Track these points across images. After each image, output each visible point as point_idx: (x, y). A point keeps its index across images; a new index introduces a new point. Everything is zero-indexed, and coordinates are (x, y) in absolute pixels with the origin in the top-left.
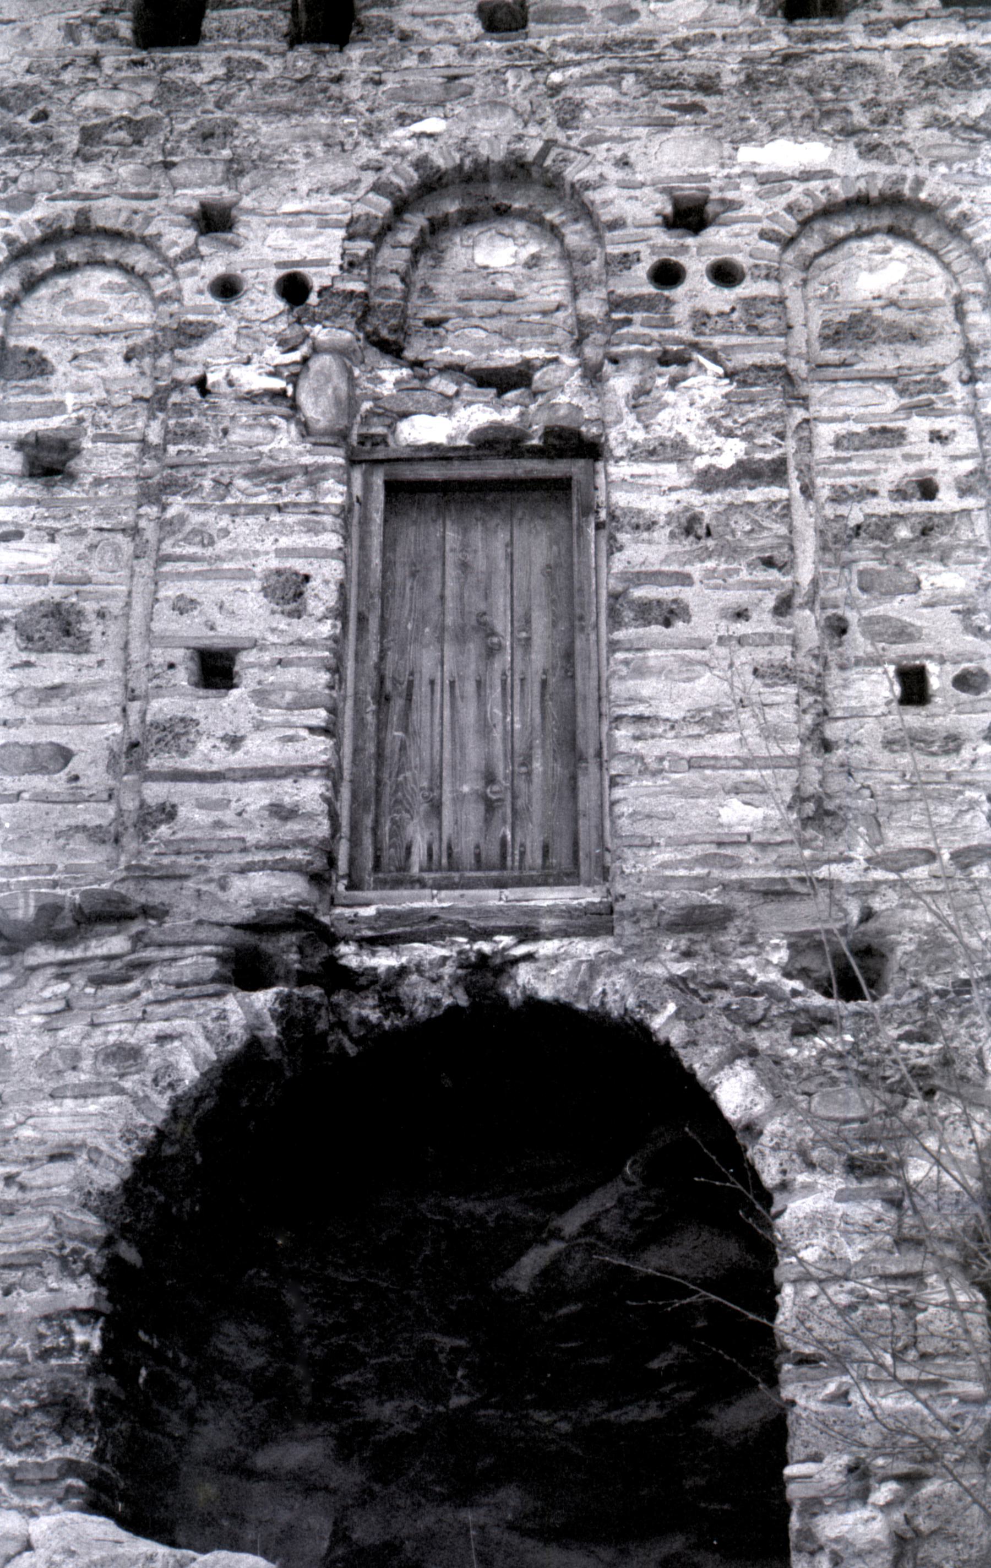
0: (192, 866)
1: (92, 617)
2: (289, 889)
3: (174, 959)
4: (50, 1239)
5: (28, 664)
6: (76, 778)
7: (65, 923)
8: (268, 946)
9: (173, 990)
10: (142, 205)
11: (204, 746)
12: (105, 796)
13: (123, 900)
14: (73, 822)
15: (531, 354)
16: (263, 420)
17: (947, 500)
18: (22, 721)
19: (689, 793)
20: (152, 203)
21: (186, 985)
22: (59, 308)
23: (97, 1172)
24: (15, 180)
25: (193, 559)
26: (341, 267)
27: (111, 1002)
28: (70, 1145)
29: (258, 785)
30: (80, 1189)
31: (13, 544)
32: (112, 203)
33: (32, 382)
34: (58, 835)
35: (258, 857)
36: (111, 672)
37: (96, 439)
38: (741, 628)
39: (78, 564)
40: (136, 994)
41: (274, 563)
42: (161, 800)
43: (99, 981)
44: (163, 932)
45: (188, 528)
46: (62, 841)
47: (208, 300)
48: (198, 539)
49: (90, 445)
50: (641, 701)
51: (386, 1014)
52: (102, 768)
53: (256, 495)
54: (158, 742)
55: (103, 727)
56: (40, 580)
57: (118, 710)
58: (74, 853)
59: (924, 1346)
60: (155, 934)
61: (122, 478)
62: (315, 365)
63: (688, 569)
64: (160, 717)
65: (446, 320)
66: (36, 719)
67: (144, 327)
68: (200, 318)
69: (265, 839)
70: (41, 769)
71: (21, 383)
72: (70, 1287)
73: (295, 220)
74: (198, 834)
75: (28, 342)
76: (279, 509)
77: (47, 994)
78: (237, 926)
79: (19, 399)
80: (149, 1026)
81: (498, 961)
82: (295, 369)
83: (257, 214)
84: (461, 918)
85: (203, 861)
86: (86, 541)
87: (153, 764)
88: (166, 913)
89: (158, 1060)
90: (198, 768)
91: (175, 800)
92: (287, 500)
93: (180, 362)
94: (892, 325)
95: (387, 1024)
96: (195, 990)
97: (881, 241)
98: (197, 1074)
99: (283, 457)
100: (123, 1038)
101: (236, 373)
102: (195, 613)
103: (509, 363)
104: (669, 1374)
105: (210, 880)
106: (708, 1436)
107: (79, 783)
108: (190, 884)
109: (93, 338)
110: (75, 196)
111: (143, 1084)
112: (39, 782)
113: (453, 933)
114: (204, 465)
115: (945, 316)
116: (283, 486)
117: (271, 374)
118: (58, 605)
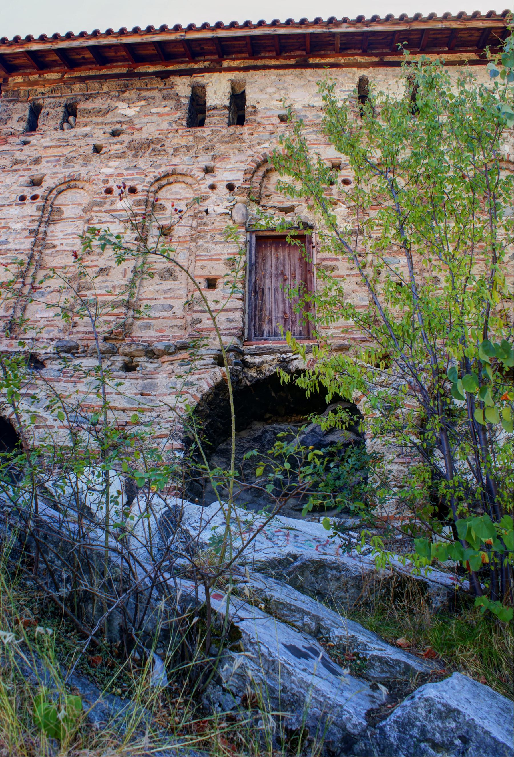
7: (172, 350)
10: (190, 167)
32: (182, 167)
38: (352, 272)
47: (208, 190)
70: (165, 311)
72: (175, 443)
73: (231, 170)
87: (195, 308)
101: (216, 208)
112: (165, 314)
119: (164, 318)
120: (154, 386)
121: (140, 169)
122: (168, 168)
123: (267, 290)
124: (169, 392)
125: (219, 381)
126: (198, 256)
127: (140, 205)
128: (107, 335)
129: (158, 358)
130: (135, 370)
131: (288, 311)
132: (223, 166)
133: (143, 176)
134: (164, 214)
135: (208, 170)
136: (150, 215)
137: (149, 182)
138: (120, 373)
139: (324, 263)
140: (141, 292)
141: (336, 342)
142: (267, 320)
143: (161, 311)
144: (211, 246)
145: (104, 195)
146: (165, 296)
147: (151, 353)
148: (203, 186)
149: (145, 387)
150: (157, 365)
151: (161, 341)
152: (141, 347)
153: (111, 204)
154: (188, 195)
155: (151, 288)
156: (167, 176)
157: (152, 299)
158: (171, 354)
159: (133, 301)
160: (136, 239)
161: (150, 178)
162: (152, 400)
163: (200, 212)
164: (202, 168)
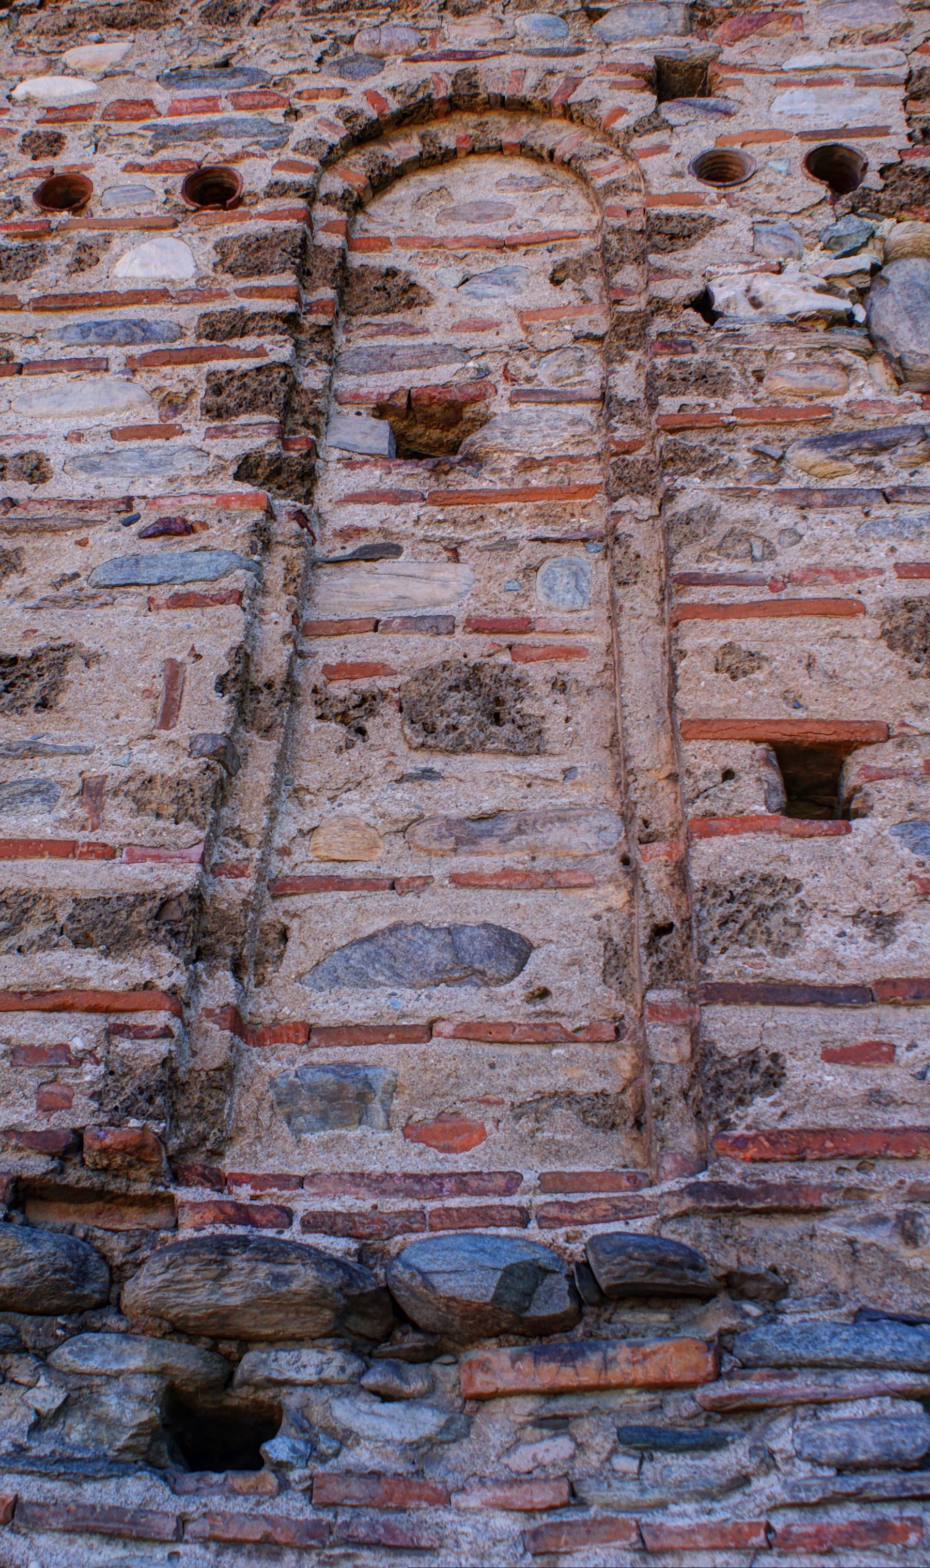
0: (831, 1188)
3: (821, 1403)
5: (428, 774)
6: (544, 994)
7: (554, 1301)
10: (564, 64)
11: (821, 932)
12: (608, 1031)
13: (694, 1261)
14: (546, 1084)
16: (825, 356)
18: (427, 881)
20: (579, 60)
21: (860, 1468)
22: (430, 214)
24: (351, 41)
25: (739, 581)
26: (910, 137)
27: (680, 1498)
31: (383, 566)
32: (510, 62)
33: (395, 318)
34: (519, 1111)
36: (593, 788)
37: (516, 398)
39: (508, 598)
40: (742, 1481)
41: (899, 589)
42: (749, 1044)
43: (645, 1442)
44: (784, 1337)
45: (721, 529)
46: (526, 1125)
47: (692, 185)
48: (742, 548)
49: (506, 408)
52: (593, 976)
53: (833, 475)
54: (724, 923)
55: (589, 893)
56: (440, 626)
57: (612, 863)
58: (556, 1151)
61: (571, 459)
62: (895, 273)
64: (719, 875)
67: (574, 236)
68: (684, 210)
71: (376, 319)
73: (815, 79)
74: (836, 1121)
75: (380, 260)
76: (887, 497)
77: (521, 1460)
79: (375, 342)
82: (863, 282)
83: (752, 70)
85: (854, 1178)
86: (518, 560)
87: (720, 968)
88: (783, 1291)
90: (818, 978)
91: (774, 1044)
92: (895, 482)
93: (660, 273)
96: (889, 1481)
99: (873, 414)
101: (764, 285)
102: (759, 676)
105: (880, 1220)
107: (553, 1004)
108: (830, 1226)
109: (493, 253)
110: (450, 55)
112: (468, 1002)
114: (729, 427)
116: (883, 459)
117: (820, 290)
118: (477, 668)
121: (254, 75)
122: (426, 69)
126: (691, 580)
127: (260, 270)
128: (37, 1165)
129: (425, 1356)
130: (253, 1461)
132: (763, 59)
133: (276, 116)
134: (409, 330)
135: (673, 82)
136: (325, 332)
137: (310, 145)
138: (136, 1490)
140: (288, 828)
143: (442, 977)
144: (769, 516)
145: (31, 213)
146: (463, 863)
147: (380, 1322)
148: (654, 165)
151: (462, 1219)
152: (304, 1278)
153: (79, 265)
154: (558, 223)
155: (354, 805)
156: (417, 112)
157: (370, 884)
159: (232, 891)
160: (246, 470)
161: (319, 124)
163: (659, 306)
164: (638, 71)
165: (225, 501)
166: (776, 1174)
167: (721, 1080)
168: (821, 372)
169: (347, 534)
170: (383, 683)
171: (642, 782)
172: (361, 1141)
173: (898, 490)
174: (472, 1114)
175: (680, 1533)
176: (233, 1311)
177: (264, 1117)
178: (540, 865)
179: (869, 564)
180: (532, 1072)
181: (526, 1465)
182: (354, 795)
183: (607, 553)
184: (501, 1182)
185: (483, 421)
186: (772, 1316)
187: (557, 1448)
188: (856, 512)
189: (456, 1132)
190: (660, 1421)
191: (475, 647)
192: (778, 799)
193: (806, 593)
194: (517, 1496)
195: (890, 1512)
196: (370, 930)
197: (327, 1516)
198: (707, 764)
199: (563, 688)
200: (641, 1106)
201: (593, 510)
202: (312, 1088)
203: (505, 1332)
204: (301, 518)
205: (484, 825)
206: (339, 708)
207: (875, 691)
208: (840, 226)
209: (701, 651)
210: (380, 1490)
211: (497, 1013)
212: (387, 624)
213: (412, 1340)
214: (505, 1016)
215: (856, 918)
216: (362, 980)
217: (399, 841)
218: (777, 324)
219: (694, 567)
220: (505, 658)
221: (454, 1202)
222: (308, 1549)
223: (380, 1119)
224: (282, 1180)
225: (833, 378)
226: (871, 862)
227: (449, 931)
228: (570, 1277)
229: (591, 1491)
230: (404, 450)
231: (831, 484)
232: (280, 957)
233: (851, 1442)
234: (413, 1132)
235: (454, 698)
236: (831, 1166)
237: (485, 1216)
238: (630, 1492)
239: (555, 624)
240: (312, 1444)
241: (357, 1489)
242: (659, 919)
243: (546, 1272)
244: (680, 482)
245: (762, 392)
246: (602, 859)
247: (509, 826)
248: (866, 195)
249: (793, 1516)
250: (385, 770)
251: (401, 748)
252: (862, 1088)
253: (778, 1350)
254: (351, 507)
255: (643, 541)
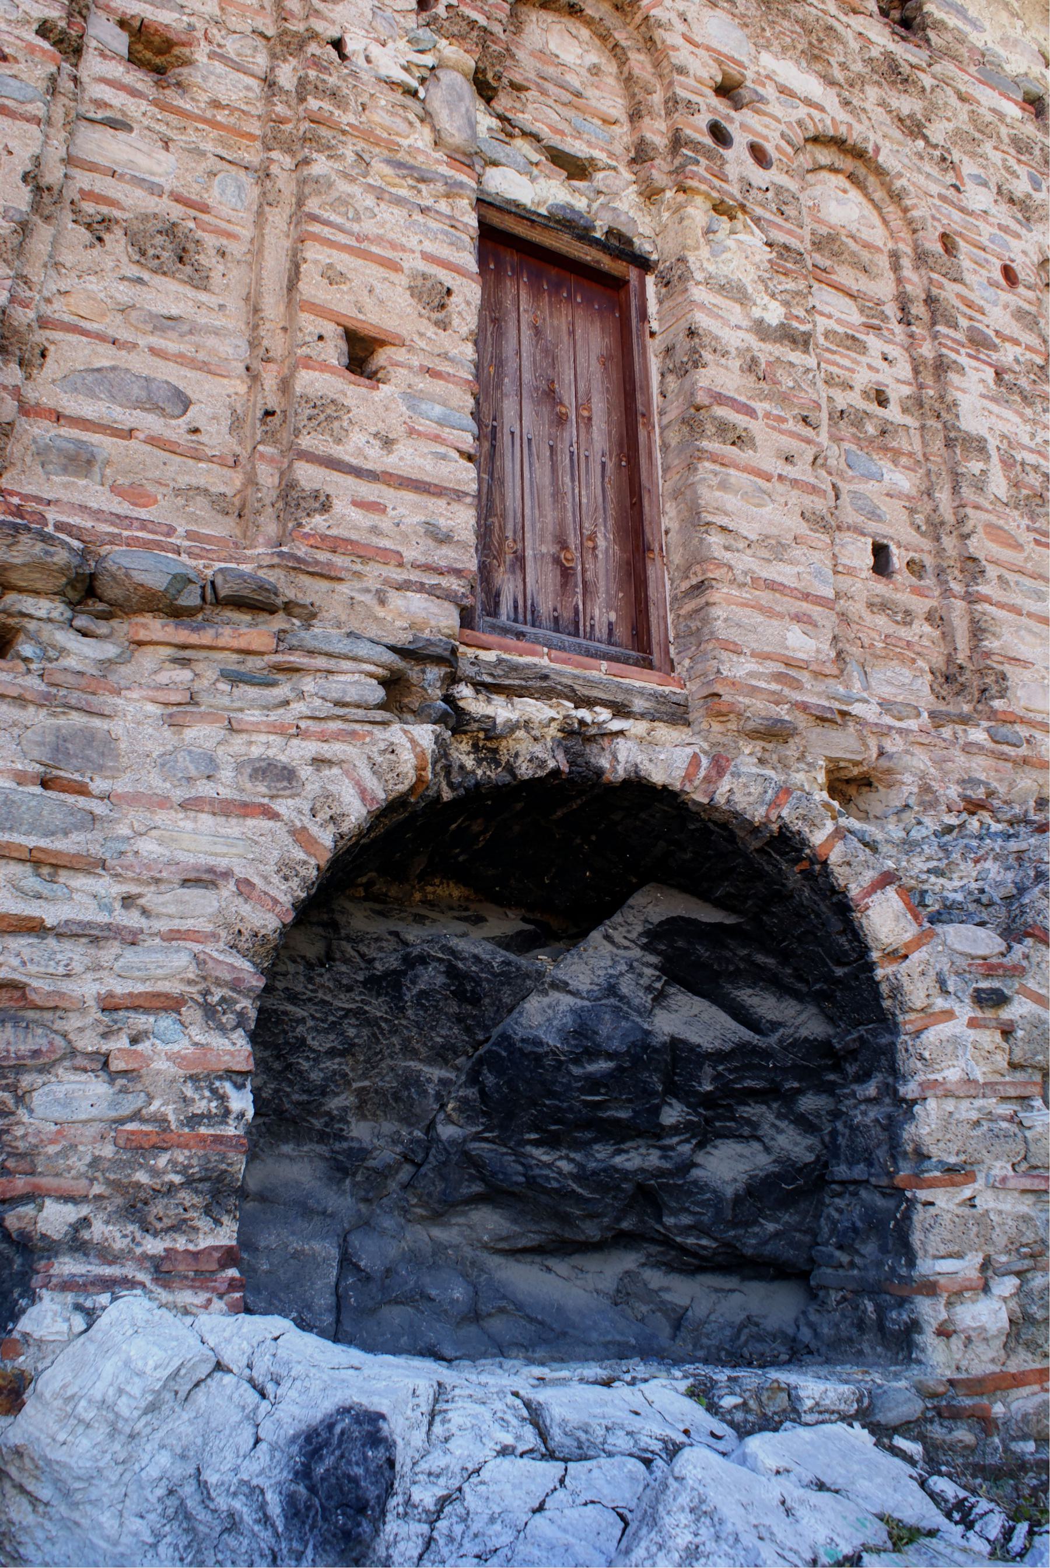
0: (348, 570)
1: (212, 252)
2: (440, 619)
3: (330, 672)
4: (190, 982)
5: (140, 281)
6: (196, 431)
7: (190, 598)
8: (413, 673)
9: (328, 709)
11: (357, 438)
14: (194, 482)
15: (596, 154)
17: (893, 413)
19: (769, 612)
21: (345, 705)
23: (247, 908)
25: (340, 229)
28: (211, 870)
29: (410, 496)
30: (228, 926)
31: (121, 135)
34: (178, 492)
35: (415, 576)
37: (212, 56)
38: (789, 471)
41: (422, 266)
42: (316, 486)
43: (235, 678)
44: (315, 637)
48: (343, 209)
49: (205, 60)
50: (726, 514)
51: (479, 761)
52: (225, 430)
53: (394, 185)
55: (225, 381)
56: (155, 190)
57: (241, 368)
59: (1034, 1161)
60: (307, 638)
63: (752, 404)
64: (310, 392)
65: (527, 89)
66: (152, 350)
69: (422, 560)
70: (157, 408)
72: (217, 1041)
74: (354, 537)
76: (423, 210)
77: (163, 678)
78: (393, 649)
80: (304, 744)
81: (593, 731)
82: (426, 73)
84: (569, 682)
85: (358, 567)
87: (306, 442)
88: (314, 616)
89: (316, 786)
90: (354, 462)
91: (329, 490)
94: (853, 254)
95: (479, 772)
96: (360, 713)
97: (840, 180)
98: (364, 812)
99: (421, 158)
100: (271, 753)
101: (375, 50)
102: (344, 287)
103: (579, 154)
104: (675, 1130)
105: (368, 591)
106: (701, 1187)
108: (343, 588)
111: (300, 812)
112: (151, 423)
113: (560, 695)
114: (344, 132)
115: (883, 262)
116: (422, 186)
118: (174, 224)
119: (153, 441)
120: (102, 751)
123: (507, 438)
124: (178, 794)
125: (403, 788)
131: (573, 541)
139: (720, 411)
141: (759, 708)
142: (509, 557)
143: (138, 405)
146: (156, 341)
149: (60, 746)
150: (110, 650)
151: (147, 545)
152: (62, 557)
155: (92, 284)
157: (101, 337)
158: (176, 613)
162: (94, 818)
165: (31, 49)
166: (322, 556)
167: (294, 501)
168: (398, 120)
169: (100, 104)
170: (117, 213)
171: (268, 325)
172: (86, 487)
173: (428, 209)
174: (150, 488)
175: (252, 723)
176: (13, 567)
177: (28, 459)
178: (201, 356)
179: (408, 245)
180: (186, 473)
181: (166, 681)
182: (93, 278)
183: (260, 182)
184: (165, 529)
185: (187, 62)
186: (308, 627)
187: (184, 675)
188: (405, 212)
189: (141, 496)
190: (242, 668)
191: (176, 212)
192: (345, 360)
193: (374, 249)
194: (162, 696)
195: (357, 727)
196: (98, 365)
197: (54, 690)
198: (311, 328)
199: (223, 254)
200: (243, 506)
201: (253, 151)
202: (60, 450)
203: (159, 610)
204: (75, 80)
205: (170, 323)
206: (88, 220)
207: (401, 317)
208: (420, 31)
209: (316, 262)
210: (83, 682)
211: (169, 434)
212: (122, 175)
213: (101, 606)
214: (174, 437)
215: (376, 435)
216: (91, 394)
217: (119, 317)
218: (379, 79)
219: (317, 211)
220: (191, 225)
221: (140, 534)
222: (42, 706)
223: (98, 478)
224: (38, 500)
225: (403, 127)
226: (387, 409)
227: (146, 379)
228: (203, 588)
229: (204, 699)
230: (133, 59)
231: (393, 190)
232: (42, 365)
233: (345, 692)
234: (114, 489)
235: (159, 240)
236: (349, 559)
237: (159, 545)
238: (226, 701)
239: (223, 214)
240: (44, 651)
241: (71, 679)
242: (269, 407)
243: (190, 581)
244: (315, 155)
245: (364, 119)
246: (234, 364)
247: (186, 328)
248: (436, 18)
249: (310, 722)
250: (113, 270)
251: (125, 259)
252: (369, 524)
253: (311, 644)
254: (103, 86)
255: (285, 183)
